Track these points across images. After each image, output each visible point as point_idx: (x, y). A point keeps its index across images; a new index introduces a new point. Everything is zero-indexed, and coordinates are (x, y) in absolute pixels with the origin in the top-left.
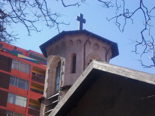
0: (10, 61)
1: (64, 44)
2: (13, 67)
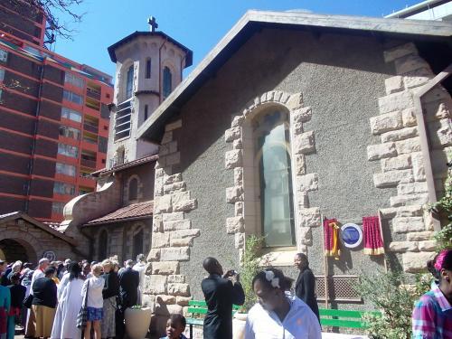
0: (63, 74)
1: (137, 47)
2: (66, 80)
